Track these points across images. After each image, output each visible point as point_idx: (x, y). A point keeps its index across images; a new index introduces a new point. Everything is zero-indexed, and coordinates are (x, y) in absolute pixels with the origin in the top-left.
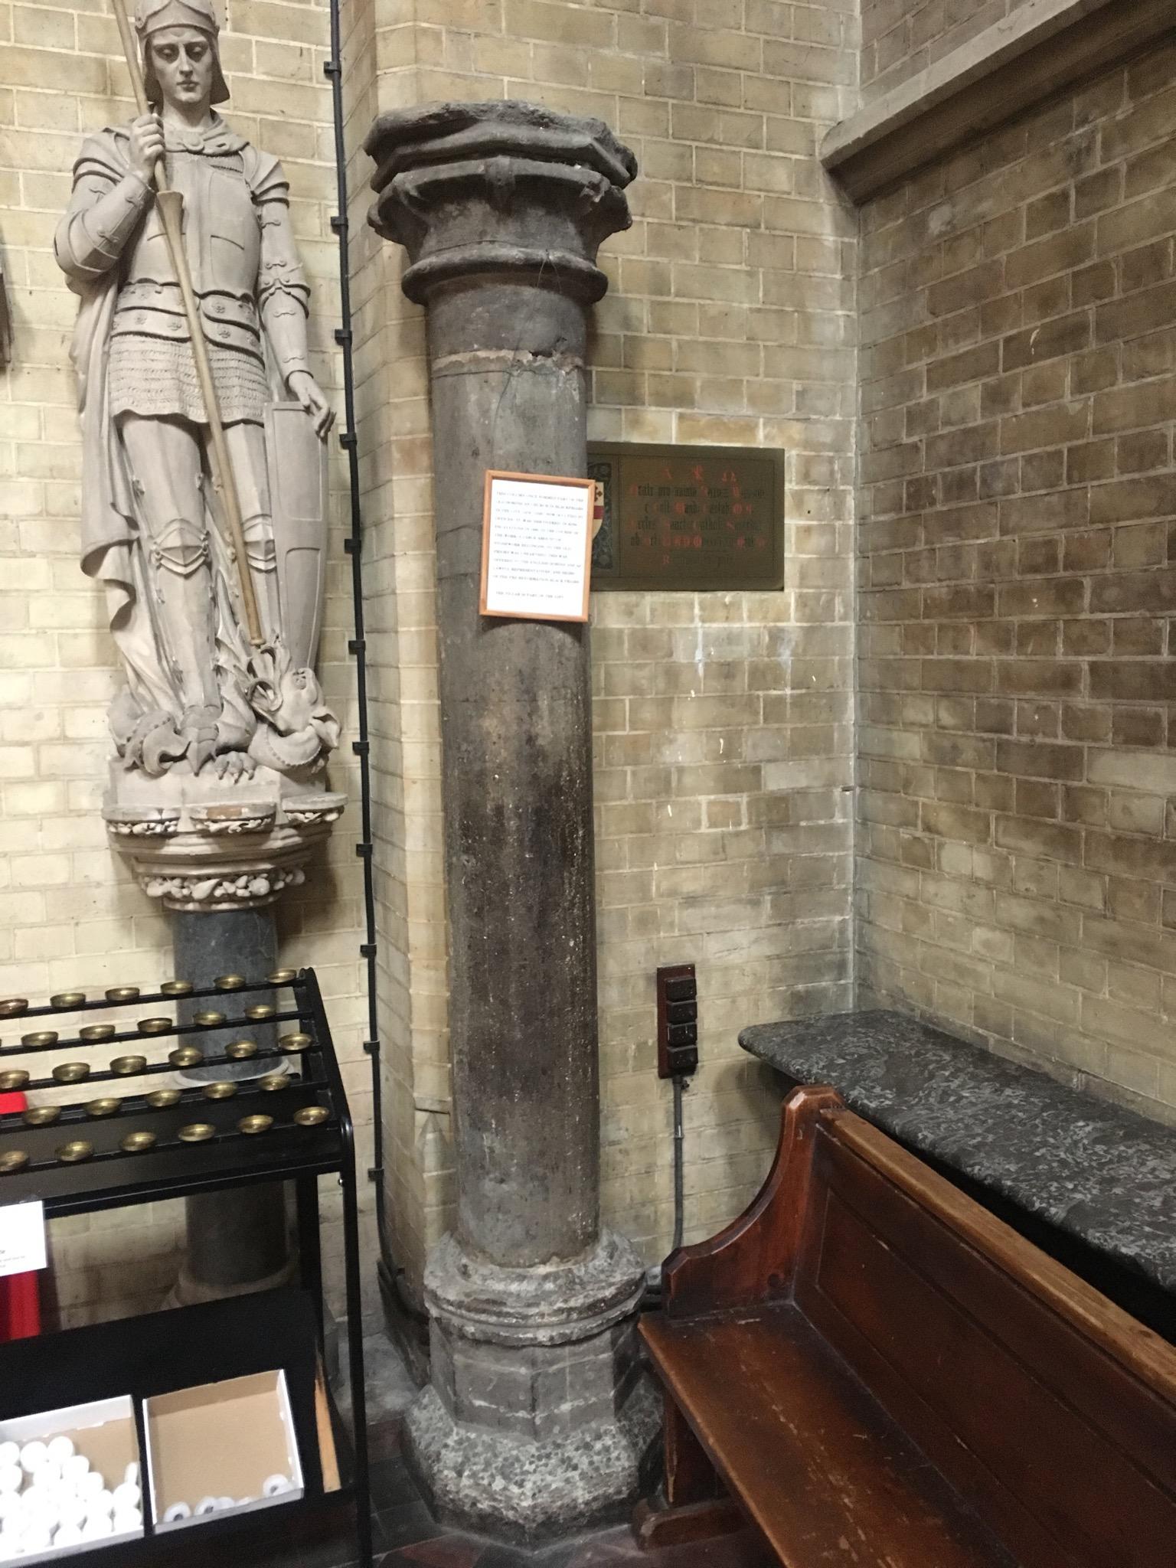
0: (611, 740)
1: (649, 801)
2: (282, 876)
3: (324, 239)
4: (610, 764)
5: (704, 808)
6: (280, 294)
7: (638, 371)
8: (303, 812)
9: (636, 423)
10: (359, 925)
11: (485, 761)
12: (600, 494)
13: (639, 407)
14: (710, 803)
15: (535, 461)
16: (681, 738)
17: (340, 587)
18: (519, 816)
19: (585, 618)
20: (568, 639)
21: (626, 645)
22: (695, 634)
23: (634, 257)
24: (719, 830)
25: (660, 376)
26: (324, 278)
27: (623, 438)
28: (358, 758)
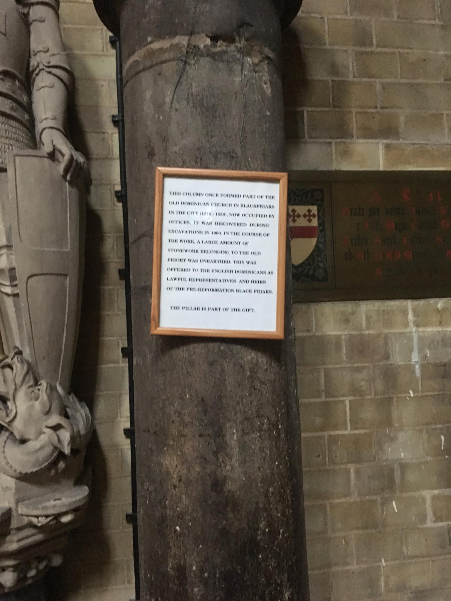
0: (333, 440)
1: (374, 498)
2: (35, 564)
3: (105, 52)
4: (333, 462)
5: (428, 502)
6: (43, 74)
7: (344, 109)
8: (37, 517)
9: (345, 154)
10: (129, 582)
11: (165, 507)
12: (314, 216)
13: (348, 141)
14: (435, 498)
15: (215, 156)
16: (402, 436)
17: (116, 305)
18: (205, 582)
19: (280, 335)
20: (262, 360)
21: (344, 350)
22: (410, 339)
23: (339, 16)
24: (444, 524)
25: (365, 113)
26: (105, 80)
27: (335, 167)
28: (129, 441)
